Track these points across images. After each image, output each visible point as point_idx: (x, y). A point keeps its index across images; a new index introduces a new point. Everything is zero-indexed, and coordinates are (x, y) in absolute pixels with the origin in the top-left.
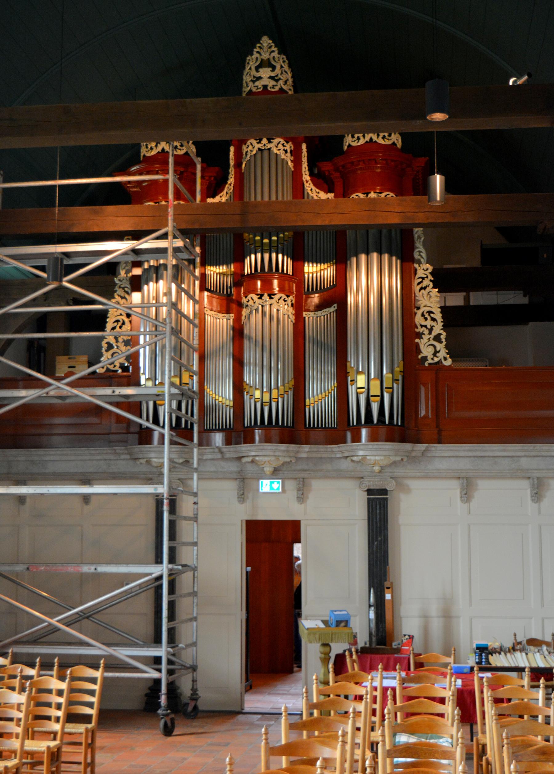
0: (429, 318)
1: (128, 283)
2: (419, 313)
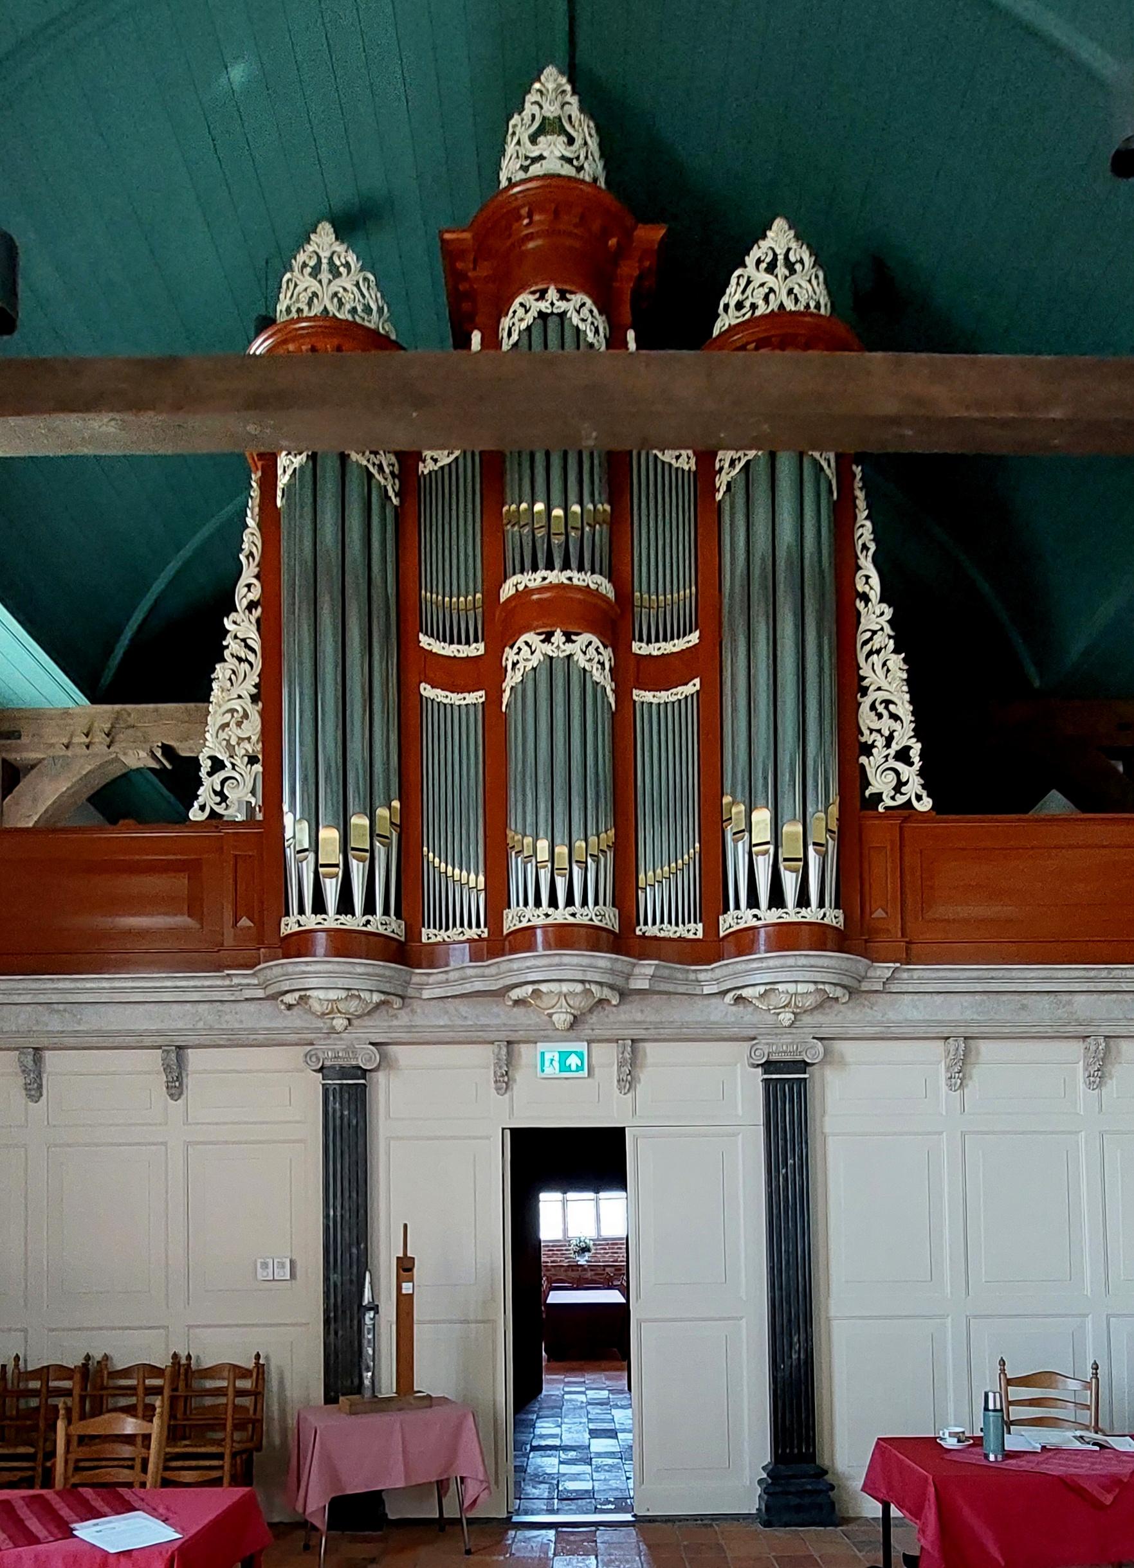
0: (885, 713)
1: (254, 628)
2: (866, 702)
